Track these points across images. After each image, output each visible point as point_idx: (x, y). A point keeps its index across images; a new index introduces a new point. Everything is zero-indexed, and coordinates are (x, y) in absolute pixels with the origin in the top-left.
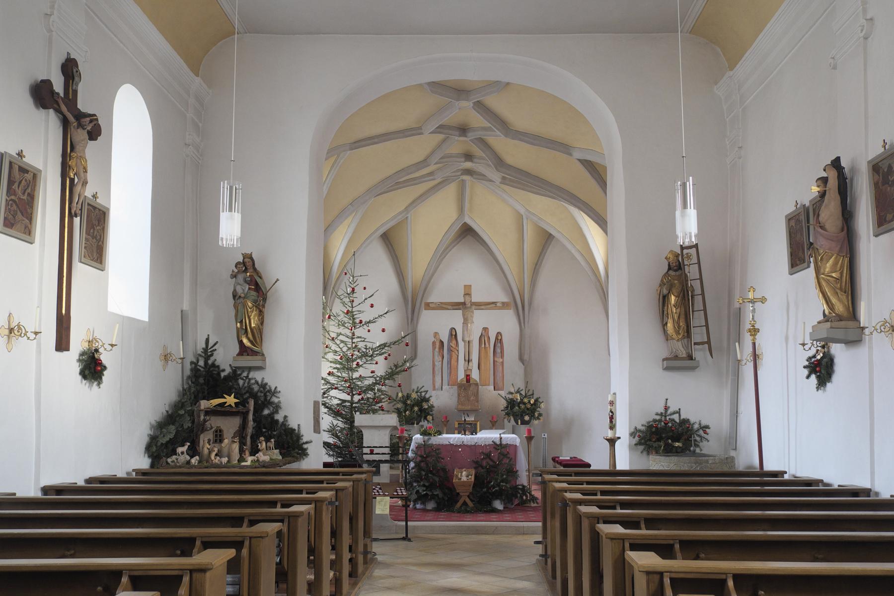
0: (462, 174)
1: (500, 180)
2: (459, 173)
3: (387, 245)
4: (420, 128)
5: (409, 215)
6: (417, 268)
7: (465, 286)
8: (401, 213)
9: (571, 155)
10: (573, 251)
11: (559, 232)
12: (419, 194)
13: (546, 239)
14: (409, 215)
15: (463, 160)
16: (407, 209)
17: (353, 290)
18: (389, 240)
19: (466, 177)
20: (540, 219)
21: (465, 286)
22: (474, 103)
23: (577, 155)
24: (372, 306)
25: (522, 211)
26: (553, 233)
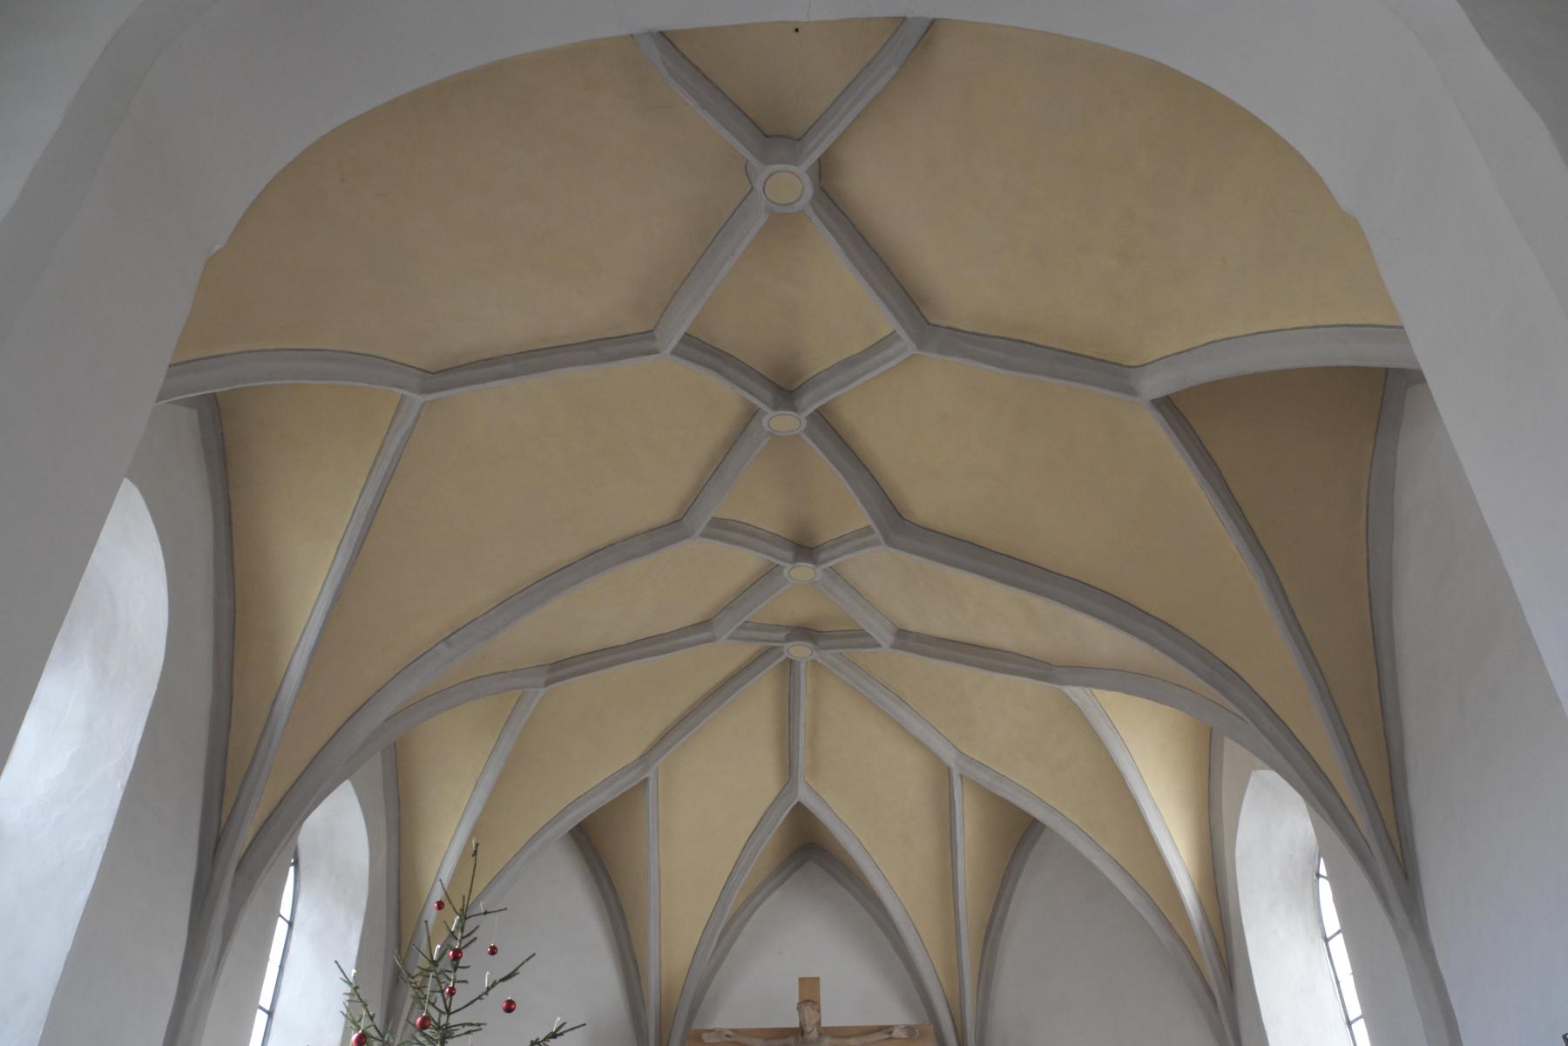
0: (788, 639)
1: (890, 638)
2: (782, 635)
3: (598, 881)
4: (649, 334)
5: (650, 774)
6: (676, 937)
7: (802, 980)
8: (634, 765)
9: (1132, 392)
10: (1097, 861)
11: (1053, 809)
12: (675, 714)
13: (1019, 834)
14: (650, 774)
15: (789, 555)
16: (646, 758)
17: (457, 955)
18: (600, 845)
19: (799, 651)
20: (999, 776)
21: (802, 980)
22: (811, 418)
23: (1156, 384)
24: (510, 1007)
25: (949, 757)
26: (1038, 812)
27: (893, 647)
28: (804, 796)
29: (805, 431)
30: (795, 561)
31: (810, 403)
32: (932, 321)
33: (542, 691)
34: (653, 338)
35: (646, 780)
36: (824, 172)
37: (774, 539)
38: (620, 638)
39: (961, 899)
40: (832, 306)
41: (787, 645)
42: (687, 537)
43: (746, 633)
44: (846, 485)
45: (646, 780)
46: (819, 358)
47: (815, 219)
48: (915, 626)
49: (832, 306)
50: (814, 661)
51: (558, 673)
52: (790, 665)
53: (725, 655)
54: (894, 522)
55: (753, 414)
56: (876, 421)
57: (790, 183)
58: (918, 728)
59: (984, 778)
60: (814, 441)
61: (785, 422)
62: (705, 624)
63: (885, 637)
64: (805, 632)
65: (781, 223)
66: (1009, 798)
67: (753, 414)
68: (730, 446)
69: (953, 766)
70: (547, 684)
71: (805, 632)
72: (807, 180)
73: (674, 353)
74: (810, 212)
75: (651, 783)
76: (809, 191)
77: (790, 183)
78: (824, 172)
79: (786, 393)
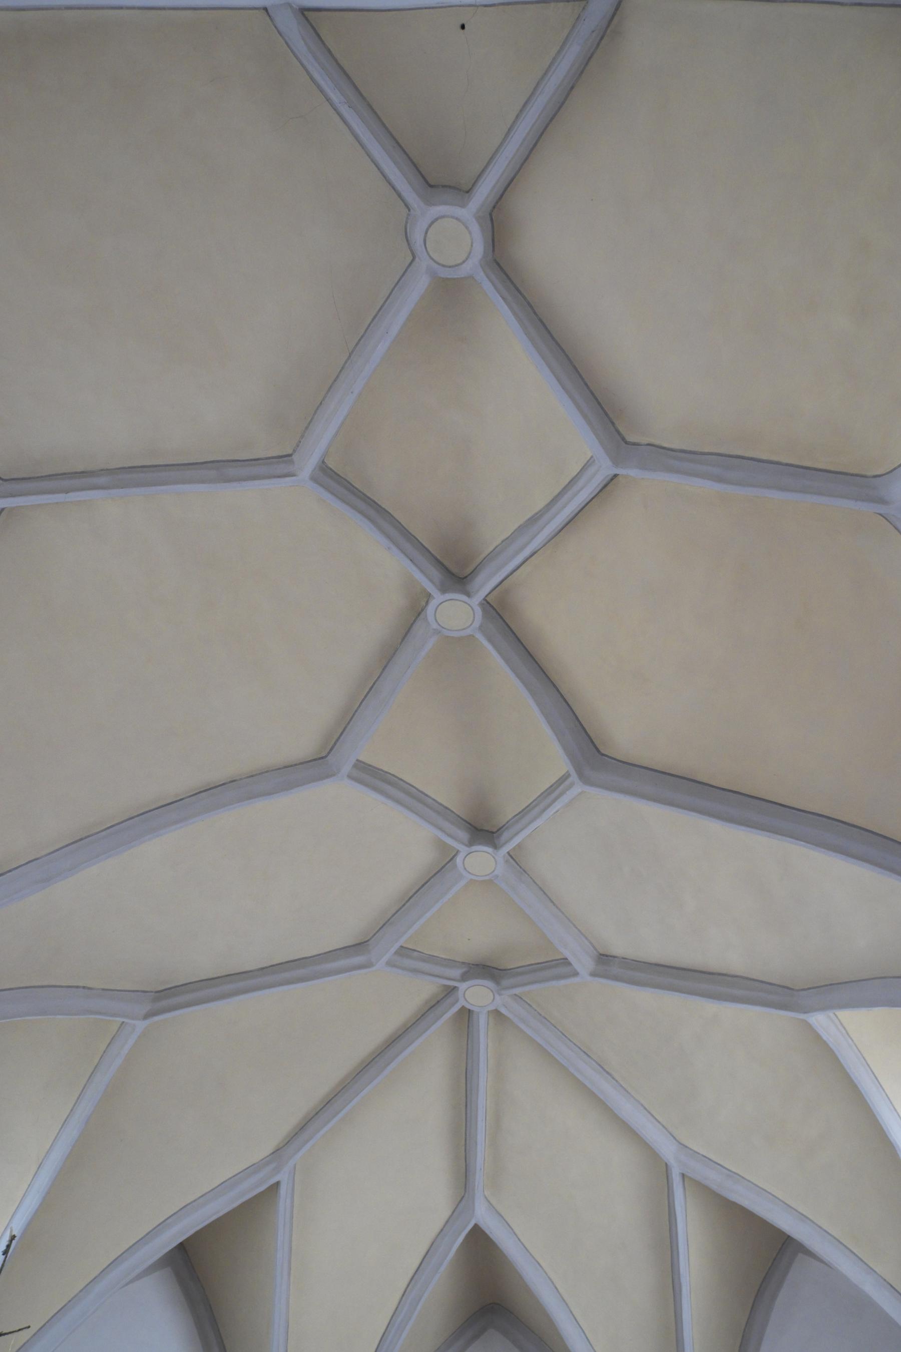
0: (464, 978)
2: (457, 973)
4: (286, 458)
5: (282, 1177)
15: (464, 835)
16: (278, 1154)
19: (478, 995)
20: (731, 1174)
25: (668, 1151)
27: (594, 974)
28: (482, 1216)
29: (481, 628)
30: (471, 843)
31: (485, 585)
32: (631, 438)
33: (141, 1025)
34: (292, 462)
35: (278, 1184)
36: (498, 225)
37: (443, 811)
38: (251, 960)
39: (686, 1316)
40: (511, 433)
41: (463, 986)
42: (328, 776)
43: (408, 962)
44: (531, 701)
45: (278, 1184)
46: (493, 531)
47: (487, 286)
48: (619, 947)
49: (511, 433)
50: (497, 1013)
51: (164, 1003)
52: (466, 1016)
53: (386, 997)
54: (592, 755)
55: (416, 609)
56: (567, 613)
57: (454, 236)
58: (626, 1109)
59: (713, 1179)
60: (490, 640)
61: (456, 613)
62: (360, 946)
63: (583, 963)
64: (486, 970)
65: (449, 291)
66: (745, 1203)
67: (416, 609)
68: (388, 655)
69: (672, 1162)
70: (146, 1017)
71: (486, 970)
72: (475, 228)
73: (390, 964)
74: (481, 276)
75: (283, 1190)
76: (479, 249)
77: (454, 236)
78: (498, 225)
79: (456, 576)
